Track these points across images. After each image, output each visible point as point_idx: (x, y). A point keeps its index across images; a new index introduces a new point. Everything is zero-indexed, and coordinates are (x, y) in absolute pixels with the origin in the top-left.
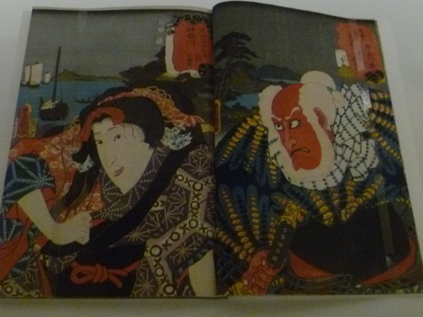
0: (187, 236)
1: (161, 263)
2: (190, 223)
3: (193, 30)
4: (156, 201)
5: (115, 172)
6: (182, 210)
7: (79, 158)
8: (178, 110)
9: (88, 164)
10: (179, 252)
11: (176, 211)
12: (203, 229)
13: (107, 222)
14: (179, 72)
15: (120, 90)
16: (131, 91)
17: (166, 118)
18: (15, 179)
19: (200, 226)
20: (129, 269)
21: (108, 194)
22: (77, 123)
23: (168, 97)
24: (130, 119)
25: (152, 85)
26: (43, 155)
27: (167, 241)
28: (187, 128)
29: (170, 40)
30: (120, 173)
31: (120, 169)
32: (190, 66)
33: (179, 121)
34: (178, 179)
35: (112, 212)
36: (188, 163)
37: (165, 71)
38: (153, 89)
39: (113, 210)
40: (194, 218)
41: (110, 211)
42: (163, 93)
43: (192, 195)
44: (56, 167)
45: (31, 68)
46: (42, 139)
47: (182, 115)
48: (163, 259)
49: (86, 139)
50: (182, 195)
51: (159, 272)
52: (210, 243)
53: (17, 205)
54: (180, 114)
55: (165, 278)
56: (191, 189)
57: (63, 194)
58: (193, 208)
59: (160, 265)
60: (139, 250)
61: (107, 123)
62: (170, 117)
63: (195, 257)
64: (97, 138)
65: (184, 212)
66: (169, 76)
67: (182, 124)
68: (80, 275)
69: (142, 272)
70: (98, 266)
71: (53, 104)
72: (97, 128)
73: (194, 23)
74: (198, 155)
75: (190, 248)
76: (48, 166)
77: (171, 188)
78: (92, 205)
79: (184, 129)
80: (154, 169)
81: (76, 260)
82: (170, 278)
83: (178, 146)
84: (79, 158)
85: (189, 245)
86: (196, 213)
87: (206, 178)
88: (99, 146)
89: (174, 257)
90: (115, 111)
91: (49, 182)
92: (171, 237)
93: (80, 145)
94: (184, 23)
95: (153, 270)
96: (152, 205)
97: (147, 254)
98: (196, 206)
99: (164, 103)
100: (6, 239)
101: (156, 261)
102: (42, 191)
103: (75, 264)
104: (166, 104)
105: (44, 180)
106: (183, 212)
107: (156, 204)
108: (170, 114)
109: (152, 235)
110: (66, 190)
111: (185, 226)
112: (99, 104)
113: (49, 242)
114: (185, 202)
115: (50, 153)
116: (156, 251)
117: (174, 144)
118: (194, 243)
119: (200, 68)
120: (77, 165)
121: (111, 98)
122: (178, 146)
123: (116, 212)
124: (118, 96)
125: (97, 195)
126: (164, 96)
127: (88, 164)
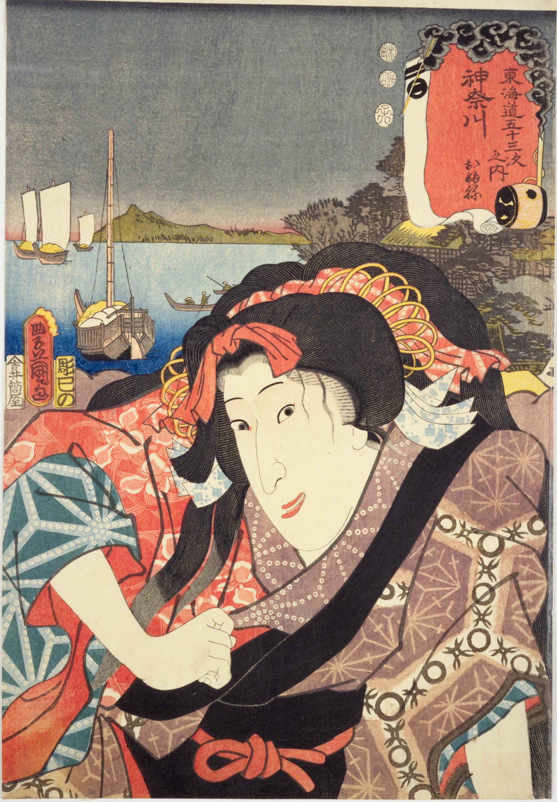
0: (462, 671)
1: (402, 734)
2: (469, 638)
3: (483, 76)
4: (385, 583)
5: (284, 507)
6: (449, 608)
7: (192, 467)
8: (440, 336)
9: (213, 488)
10: (440, 710)
11: (436, 609)
12: (503, 651)
13: (271, 636)
14: (441, 220)
15: (288, 271)
16: (313, 275)
17: (408, 359)
18: (35, 524)
19: (494, 645)
20: (329, 748)
21: (269, 563)
22: (178, 368)
23: (413, 297)
24: (316, 361)
25: (369, 260)
26: (102, 456)
27: (415, 684)
28: (463, 384)
29: (416, 110)
30: (297, 510)
31: (296, 500)
32: (471, 197)
33: (445, 367)
34: (441, 527)
35: (280, 610)
36: (467, 483)
37: (405, 218)
38: (374, 272)
39: (282, 606)
40: (481, 625)
41: (276, 607)
42: (402, 283)
43: (474, 568)
44: (137, 491)
45: (38, 195)
46: (95, 414)
47: (452, 348)
48: (406, 725)
49: (205, 412)
50: (450, 570)
51: (399, 756)
52: (522, 686)
53: (50, 589)
54: (445, 347)
55: (411, 770)
56: (472, 554)
57: (160, 564)
58: (478, 601)
59: (400, 740)
60: (345, 708)
61: (256, 369)
62: (419, 355)
63: (481, 719)
64: (233, 411)
65: (454, 611)
66: (415, 230)
67: (452, 374)
68: (216, 762)
69: (355, 757)
70: (256, 740)
71: (110, 311)
72: (233, 383)
73: (484, 53)
74: (493, 463)
75: (464, 701)
76: (115, 486)
77: (424, 550)
78: (233, 593)
79: (456, 389)
80: (379, 501)
81: (205, 725)
82: (422, 769)
83: (441, 436)
84: (192, 467)
85: (464, 693)
86: (485, 614)
87: (511, 522)
88: (241, 437)
89: (430, 723)
90: (274, 335)
91: (120, 530)
92: (424, 672)
93: (192, 431)
94: (456, 57)
95: (384, 751)
96: (378, 594)
97: (368, 715)
98: (485, 595)
99: (403, 313)
100: (33, 677)
101: (390, 729)
102: (107, 556)
103: (202, 737)
104: (408, 319)
105: (108, 526)
106: (451, 612)
107: (386, 592)
108: (420, 346)
109: (377, 670)
110: (167, 552)
111: (458, 645)
112: (232, 313)
113: (138, 684)
114: (458, 586)
115: (117, 452)
116: (390, 707)
117: (429, 431)
118: (478, 688)
119: (501, 201)
120: (188, 488)
121: (263, 297)
122: (441, 436)
123: (291, 613)
124: (280, 292)
125: (242, 565)
126: (404, 291)
127: (213, 488)
